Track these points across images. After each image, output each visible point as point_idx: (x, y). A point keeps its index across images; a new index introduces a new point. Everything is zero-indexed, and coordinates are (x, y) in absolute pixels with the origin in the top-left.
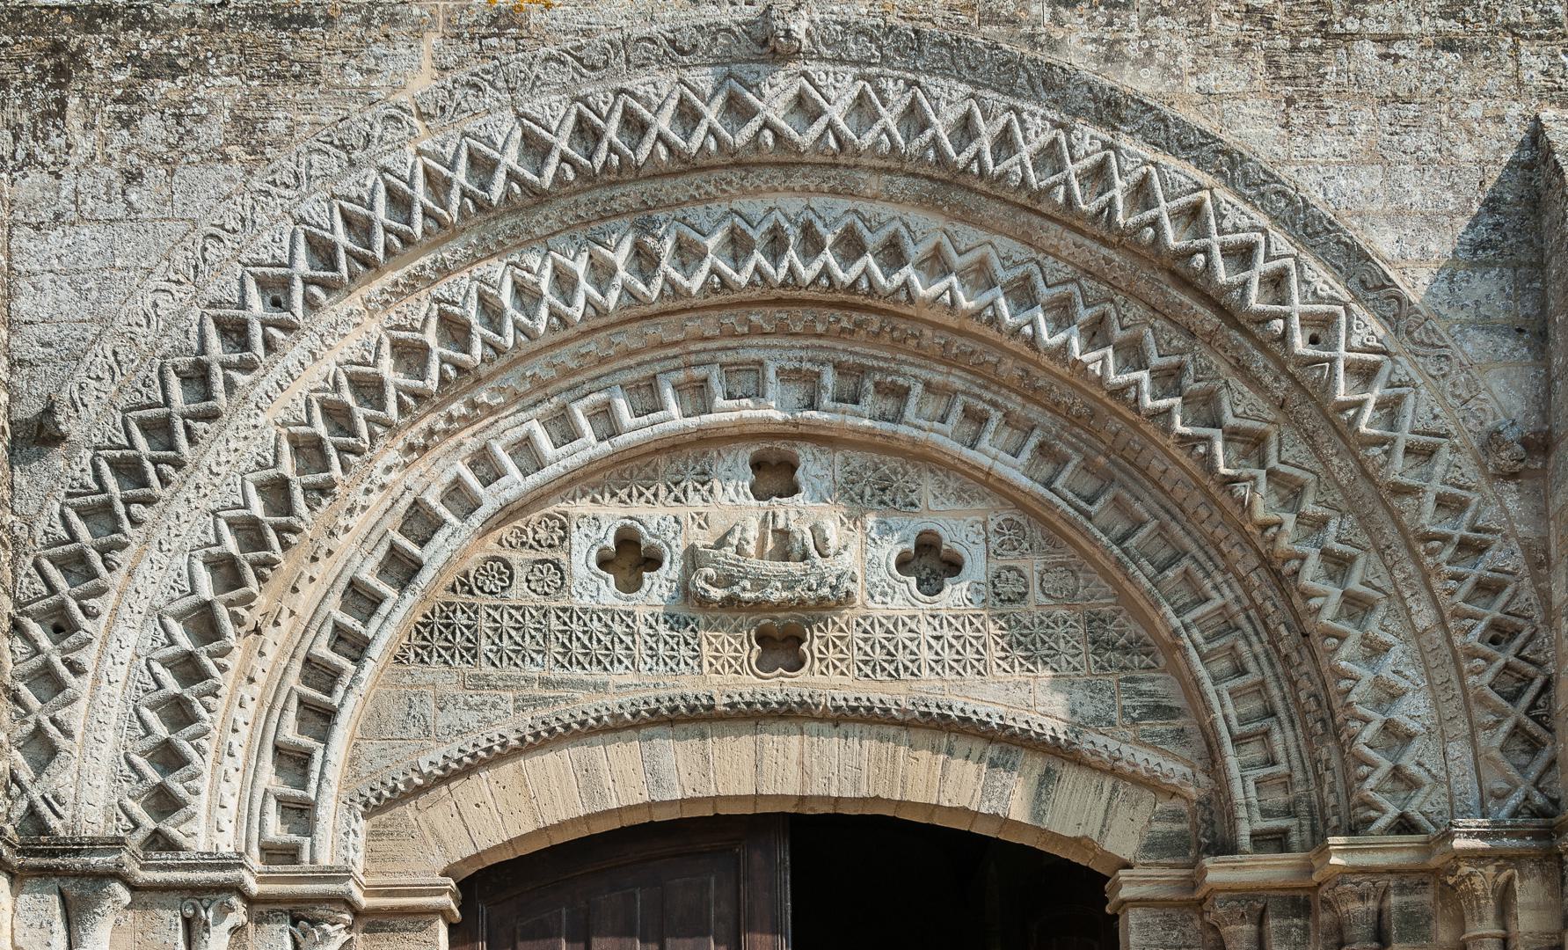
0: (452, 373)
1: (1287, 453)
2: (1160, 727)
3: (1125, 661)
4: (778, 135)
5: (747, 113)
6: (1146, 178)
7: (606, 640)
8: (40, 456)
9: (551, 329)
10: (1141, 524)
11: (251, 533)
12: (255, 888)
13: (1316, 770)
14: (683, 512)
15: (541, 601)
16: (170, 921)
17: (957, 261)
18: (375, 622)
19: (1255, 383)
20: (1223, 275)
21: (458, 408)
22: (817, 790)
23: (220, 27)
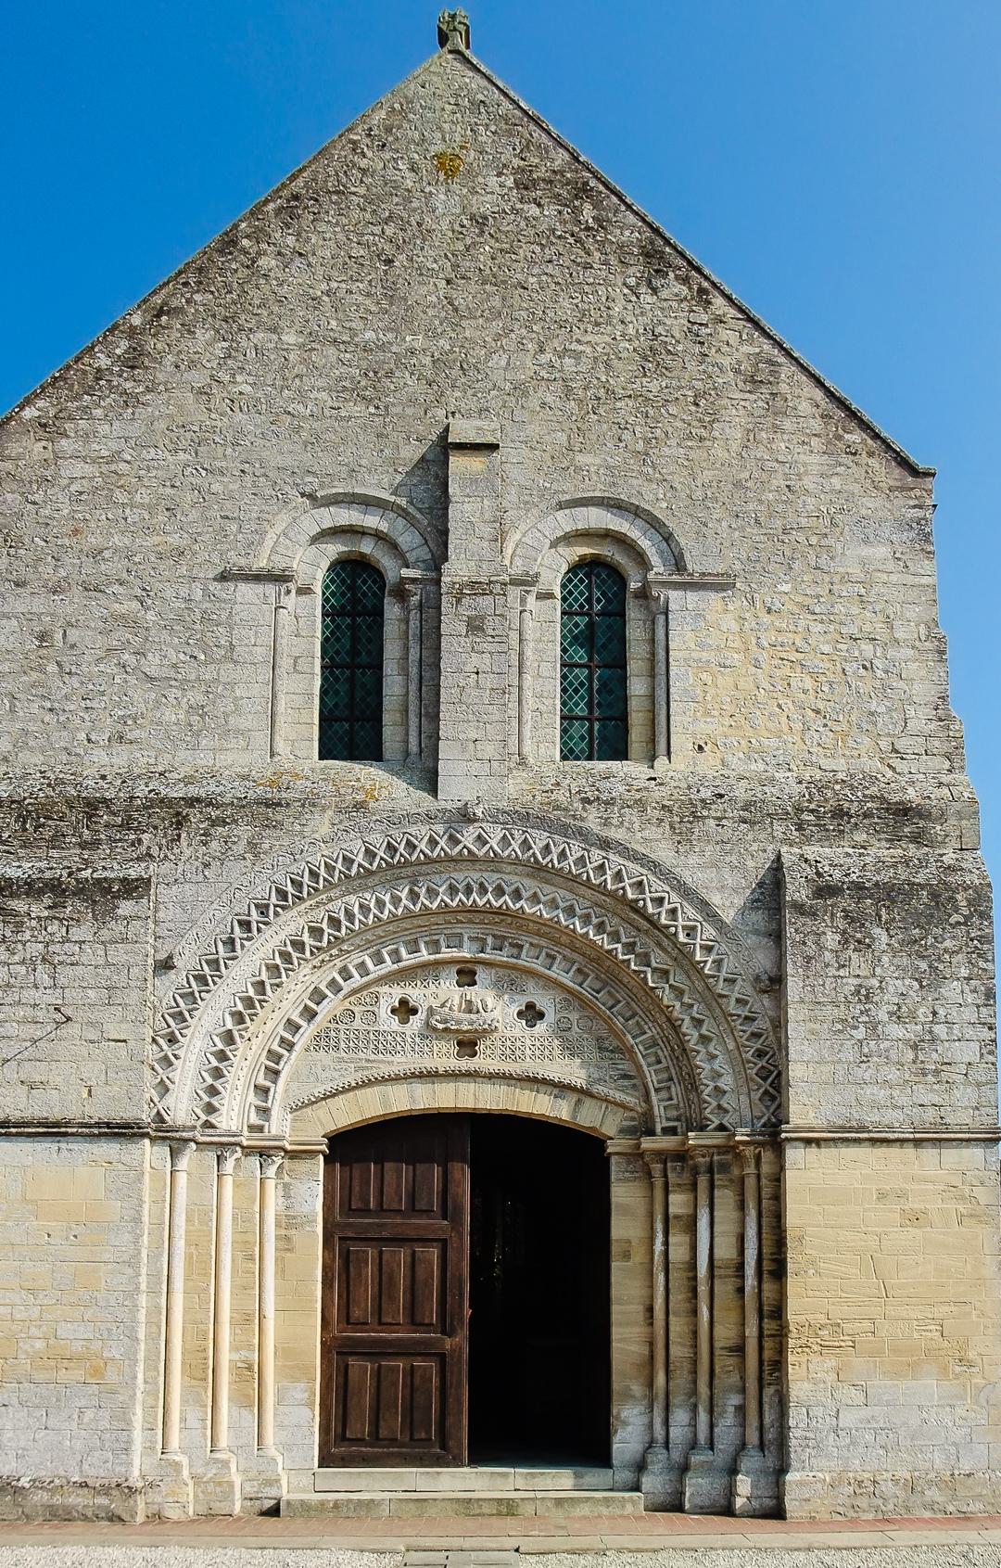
0: (333, 940)
1: (677, 979)
2: (626, 1083)
3: (612, 1056)
4: (469, 851)
5: (458, 842)
6: (620, 870)
7: (393, 1044)
8: (165, 973)
9: (374, 921)
10: (619, 1002)
11: (249, 1003)
12: (245, 1143)
13: (689, 1103)
14: (427, 992)
15: (367, 1027)
16: (211, 1156)
17: (543, 898)
18: (298, 1036)
19: (664, 950)
20: (650, 910)
21: (335, 952)
22: (480, 1106)
23: (244, 807)
